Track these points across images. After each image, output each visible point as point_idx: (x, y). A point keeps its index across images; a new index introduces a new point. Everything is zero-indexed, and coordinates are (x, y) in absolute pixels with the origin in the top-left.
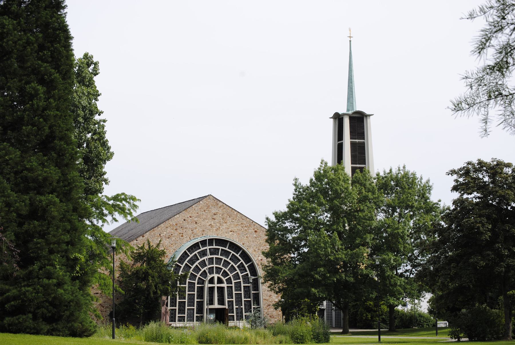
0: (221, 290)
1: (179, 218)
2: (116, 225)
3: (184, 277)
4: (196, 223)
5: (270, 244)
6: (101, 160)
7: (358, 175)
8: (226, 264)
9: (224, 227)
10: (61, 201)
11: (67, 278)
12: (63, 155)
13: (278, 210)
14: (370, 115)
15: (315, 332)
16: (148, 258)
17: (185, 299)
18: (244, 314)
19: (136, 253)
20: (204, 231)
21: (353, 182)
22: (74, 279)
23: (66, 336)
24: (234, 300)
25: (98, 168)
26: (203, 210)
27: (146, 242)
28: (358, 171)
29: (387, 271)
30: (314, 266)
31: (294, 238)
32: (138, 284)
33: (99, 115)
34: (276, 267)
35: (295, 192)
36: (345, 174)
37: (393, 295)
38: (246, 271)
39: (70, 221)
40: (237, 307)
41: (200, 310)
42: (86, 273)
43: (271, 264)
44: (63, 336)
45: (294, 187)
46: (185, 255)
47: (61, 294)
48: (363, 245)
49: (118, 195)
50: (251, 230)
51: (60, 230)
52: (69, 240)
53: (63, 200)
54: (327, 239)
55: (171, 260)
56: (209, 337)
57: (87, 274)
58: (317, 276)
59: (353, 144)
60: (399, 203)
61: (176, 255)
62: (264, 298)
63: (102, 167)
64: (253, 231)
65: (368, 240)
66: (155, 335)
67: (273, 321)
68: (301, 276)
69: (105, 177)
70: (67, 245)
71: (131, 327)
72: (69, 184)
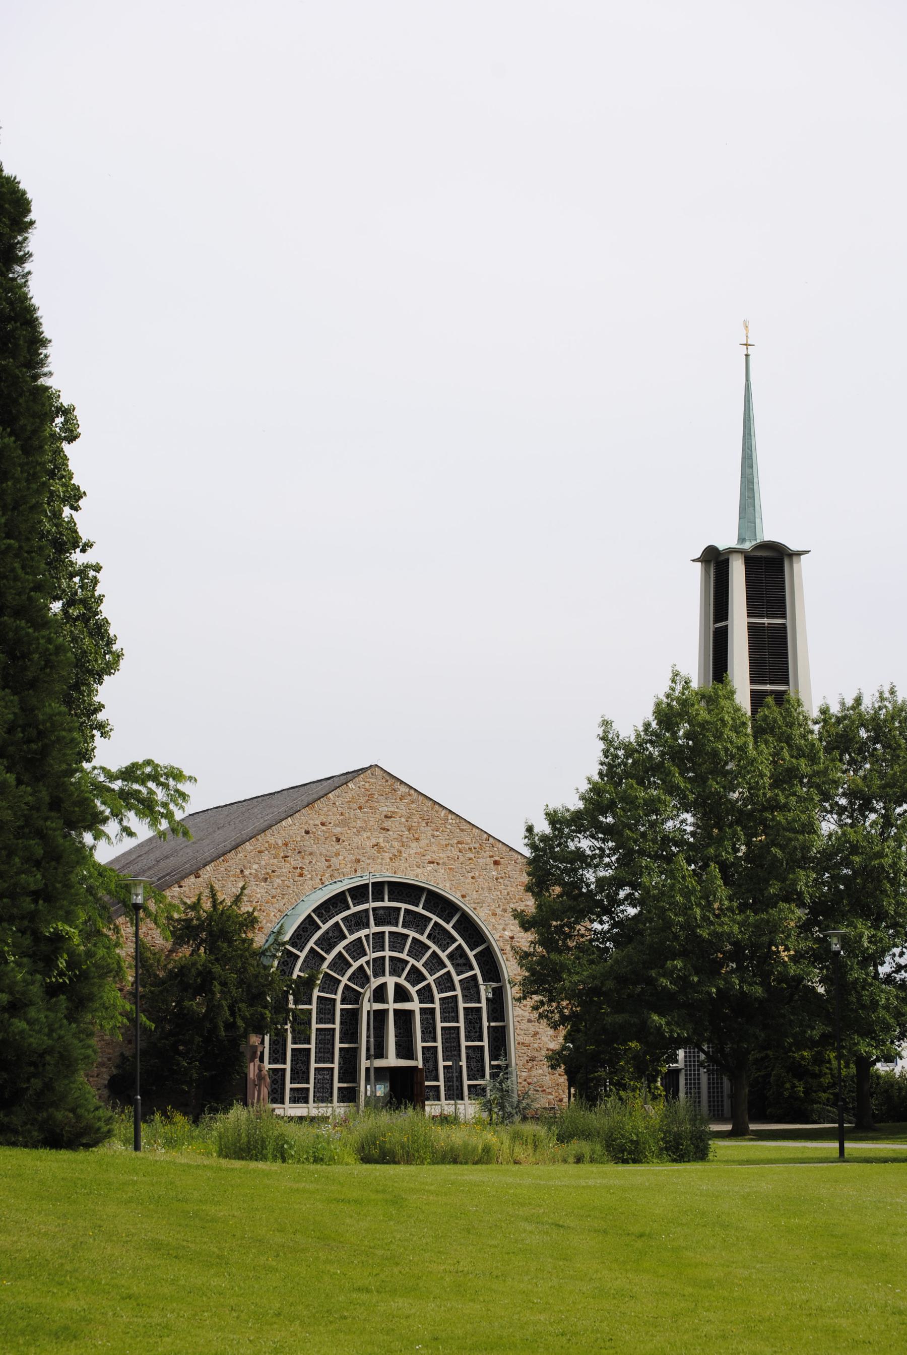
0: (404, 1018)
1: (291, 828)
2: (129, 843)
3: (307, 985)
4: (338, 840)
5: (537, 895)
6: (91, 672)
7: (772, 711)
8: (418, 949)
9: (412, 852)
10: (19, 782)
11: (36, 990)
12: (24, 656)
13: (556, 804)
14: (799, 554)
15: (670, 1132)
16: (210, 933)
17: (309, 1043)
18: (466, 1083)
19: (179, 920)
20: (358, 861)
21: (759, 732)
22: (52, 991)
23: (35, 1146)
24: (439, 1044)
25: (81, 693)
26: (355, 806)
27: (207, 892)
28: (770, 700)
29: (851, 969)
30: (659, 956)
31: (600, 881)
32: (186, 1003)
33: (83, 551)
34: (554, 956)
35: (603, 759)
36: (737, 710)
37: (868, 1032)
38: (472, 969)
39: (41, 834)
40: (450, 1063)
41: (349, 1071)
42: (84, 976)
43: (540, 949)
44: (26, 1146)
45: (601, 745)
46: (308, 926)
47: (22, 1032)
48: (787, 900)
49: (134, 766)
50: (484, 860)
51: (17, 860)
52: (41, 885)
53: (26, 778)
54: (692, 882)
55: (271, 940)
56: (388, 1146)
57: (87, 978)
58: (665, 982)
59: (754, 631)
60: (883, 787)
61: (286, 927)
62: (519, 1038)
63: (91, 692)
64: (490, 861)
65: (801, 886)
66: (244, 1139)
67: (542, 1102)
68: (622, 980)
69: (101, 716)
70: (36, 901)
71: (179, 1118)
72: (41, 734)
